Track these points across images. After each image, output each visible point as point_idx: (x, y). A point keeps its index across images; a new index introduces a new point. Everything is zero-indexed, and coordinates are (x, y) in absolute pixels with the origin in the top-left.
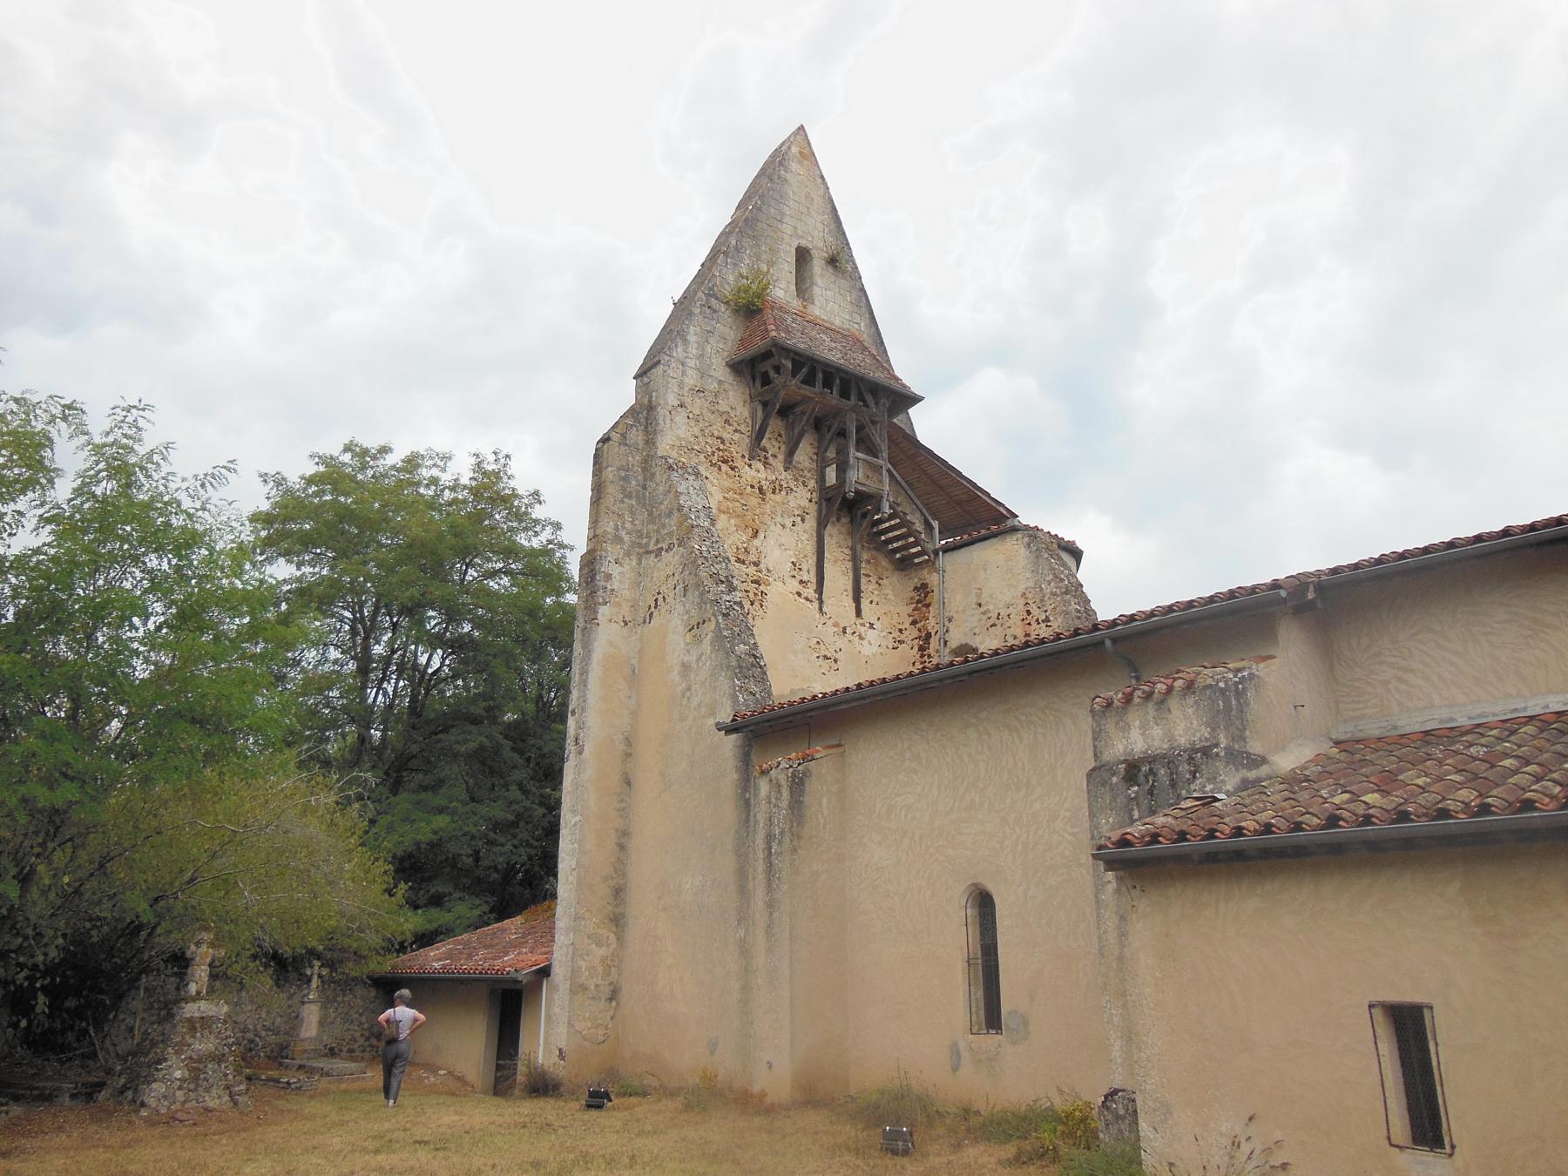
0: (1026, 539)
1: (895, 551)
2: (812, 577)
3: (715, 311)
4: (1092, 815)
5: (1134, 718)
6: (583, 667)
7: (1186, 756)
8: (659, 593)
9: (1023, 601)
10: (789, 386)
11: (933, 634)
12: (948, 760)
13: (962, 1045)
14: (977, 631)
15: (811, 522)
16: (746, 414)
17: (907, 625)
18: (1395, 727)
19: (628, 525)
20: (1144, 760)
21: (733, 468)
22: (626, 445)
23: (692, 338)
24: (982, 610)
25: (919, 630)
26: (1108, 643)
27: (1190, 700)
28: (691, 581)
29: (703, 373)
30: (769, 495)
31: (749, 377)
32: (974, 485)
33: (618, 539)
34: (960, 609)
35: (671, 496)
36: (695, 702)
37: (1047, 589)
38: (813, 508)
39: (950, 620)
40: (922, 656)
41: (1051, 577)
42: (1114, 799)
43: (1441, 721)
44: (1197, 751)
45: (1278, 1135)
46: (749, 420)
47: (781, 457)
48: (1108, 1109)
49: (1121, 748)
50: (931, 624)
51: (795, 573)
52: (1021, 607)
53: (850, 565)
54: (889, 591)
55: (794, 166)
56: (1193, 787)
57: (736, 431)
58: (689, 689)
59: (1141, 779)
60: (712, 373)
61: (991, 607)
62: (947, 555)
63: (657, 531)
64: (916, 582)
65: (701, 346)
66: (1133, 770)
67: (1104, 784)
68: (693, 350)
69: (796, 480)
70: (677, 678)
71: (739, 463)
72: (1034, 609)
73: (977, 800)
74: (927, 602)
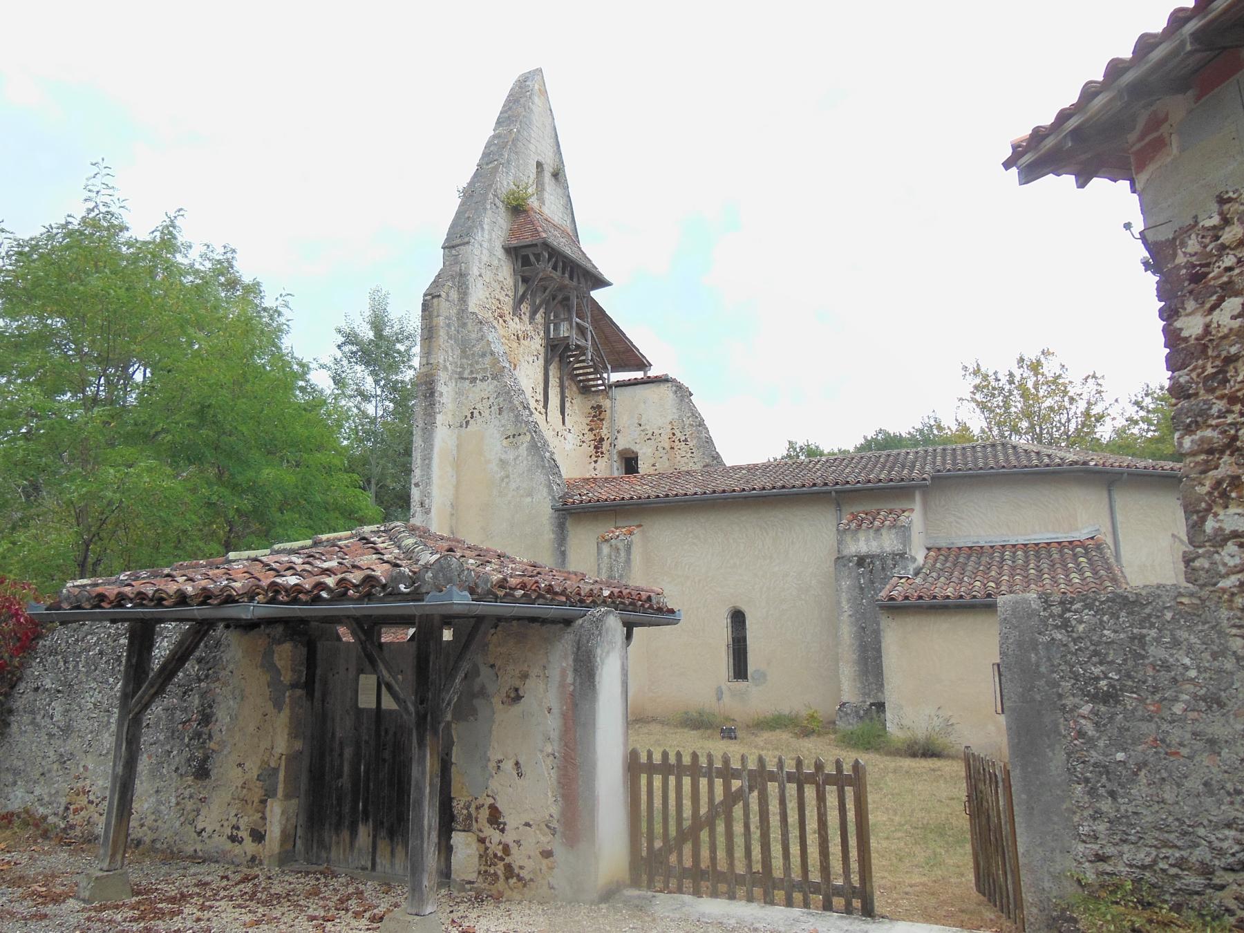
0: (674, 388)
1: (581, 381)
2: (541, 397)
3: (497, 207)
4: (837, 580)
5: (862, 536)
6: (425, 455)
7: (891, 556)
8: (474, 408)
9: (670, 427)
10: (545, 268)
11: (605, 439)
12: (720, 540)
13: (724, 688)
14: (638, 441)
15: (541, 361)
16: (512, 284)
17: (586, 431)
18: (953, 543)
19: (450, 359)
20: (868, 556)
21: (505, 321)
22: (448, 301)
23: (486, 227)
24: (642, 428)
25: (595, 435)
26: (833, 493)
27: (894, 531)
28: (506, 406)
29: (491, 254)
30: (522, 341)
31: (514, 256)
32: (631, 343)
33: (445, 368)
34: (626, 425)
35: (484, 343)
36: (513, 486)
37: (687, 422)
38: (542, 350)
39: (618, 432)
40: (597, 452)
41: (690, 414)
42: (850, 573)
43: (974, 543)
44: (897, 555)
45: (950, 714)
46: (513, 288)
47: (528, 314)
48: (842, 711)
49: (854, 550)
50: (604, 432)
51: (533, 395)
52: (669, 430)
53: (558, 389)
54: (576, 408)
55: (536, 99)
56: (894, 571)
57: (506, 295)
58: (507, 477)
59: (866, 565)
60: (495, 253)
61: (648, 427)
62: (618, 389)
63: (471, 365)
64: (593, 403)
65: (490, 233)
66: (861, 561)
67: (845, 566)
68: (486, 236)
69: (535, 331)
70: (496, 468)
71: (507, 318)
72: (678, 434)
73: (738, 563)
74: (602, 417)
